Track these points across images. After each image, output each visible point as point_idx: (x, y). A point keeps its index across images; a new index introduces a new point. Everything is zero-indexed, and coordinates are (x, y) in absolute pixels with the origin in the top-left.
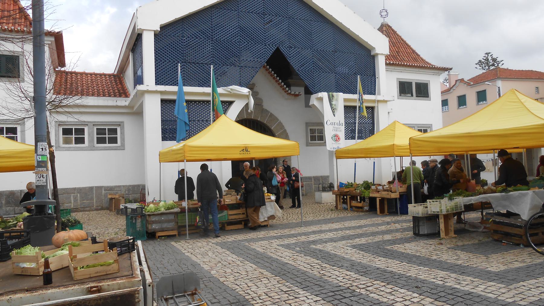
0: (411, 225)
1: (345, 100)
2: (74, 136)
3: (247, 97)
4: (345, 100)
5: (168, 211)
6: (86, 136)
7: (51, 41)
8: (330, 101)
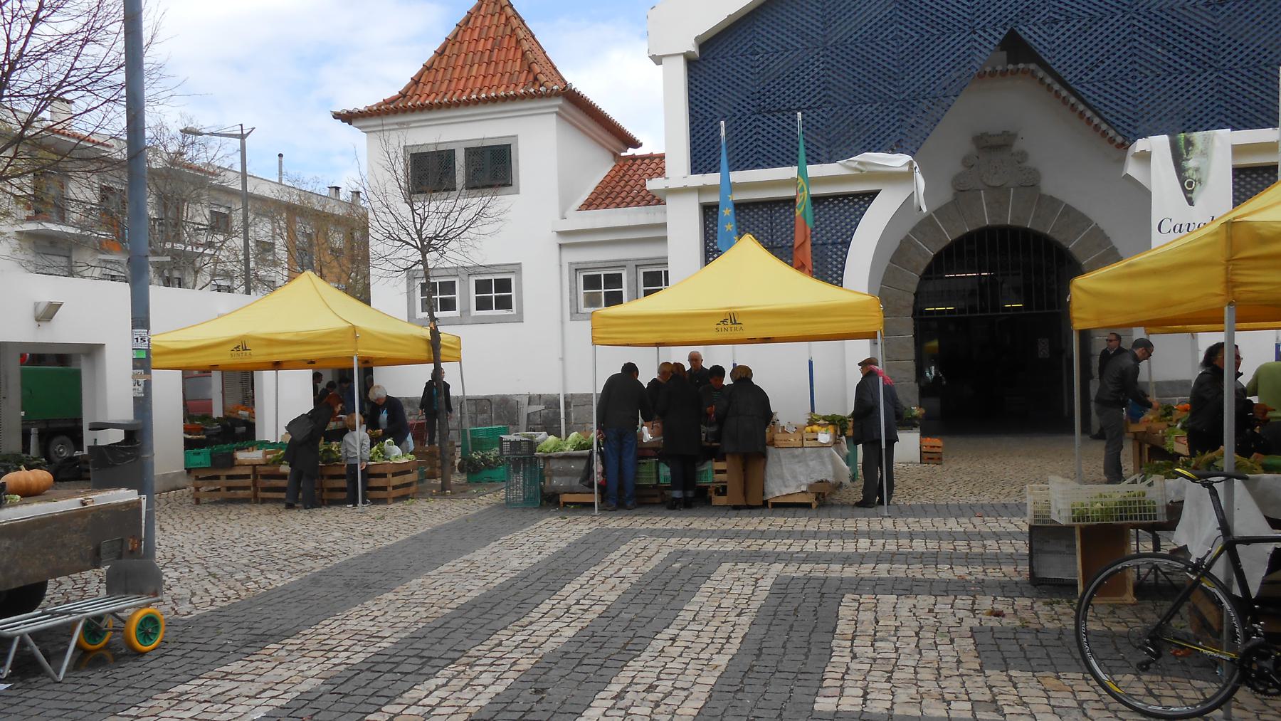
0: (1023, 547)
1: (1237, 150)
2: (603, 290)
3: (906, 177)
4: (1237, 150)
5: (578, 452)
6: (473, 296)
7: (559, 107)
8: (1178, 158)
